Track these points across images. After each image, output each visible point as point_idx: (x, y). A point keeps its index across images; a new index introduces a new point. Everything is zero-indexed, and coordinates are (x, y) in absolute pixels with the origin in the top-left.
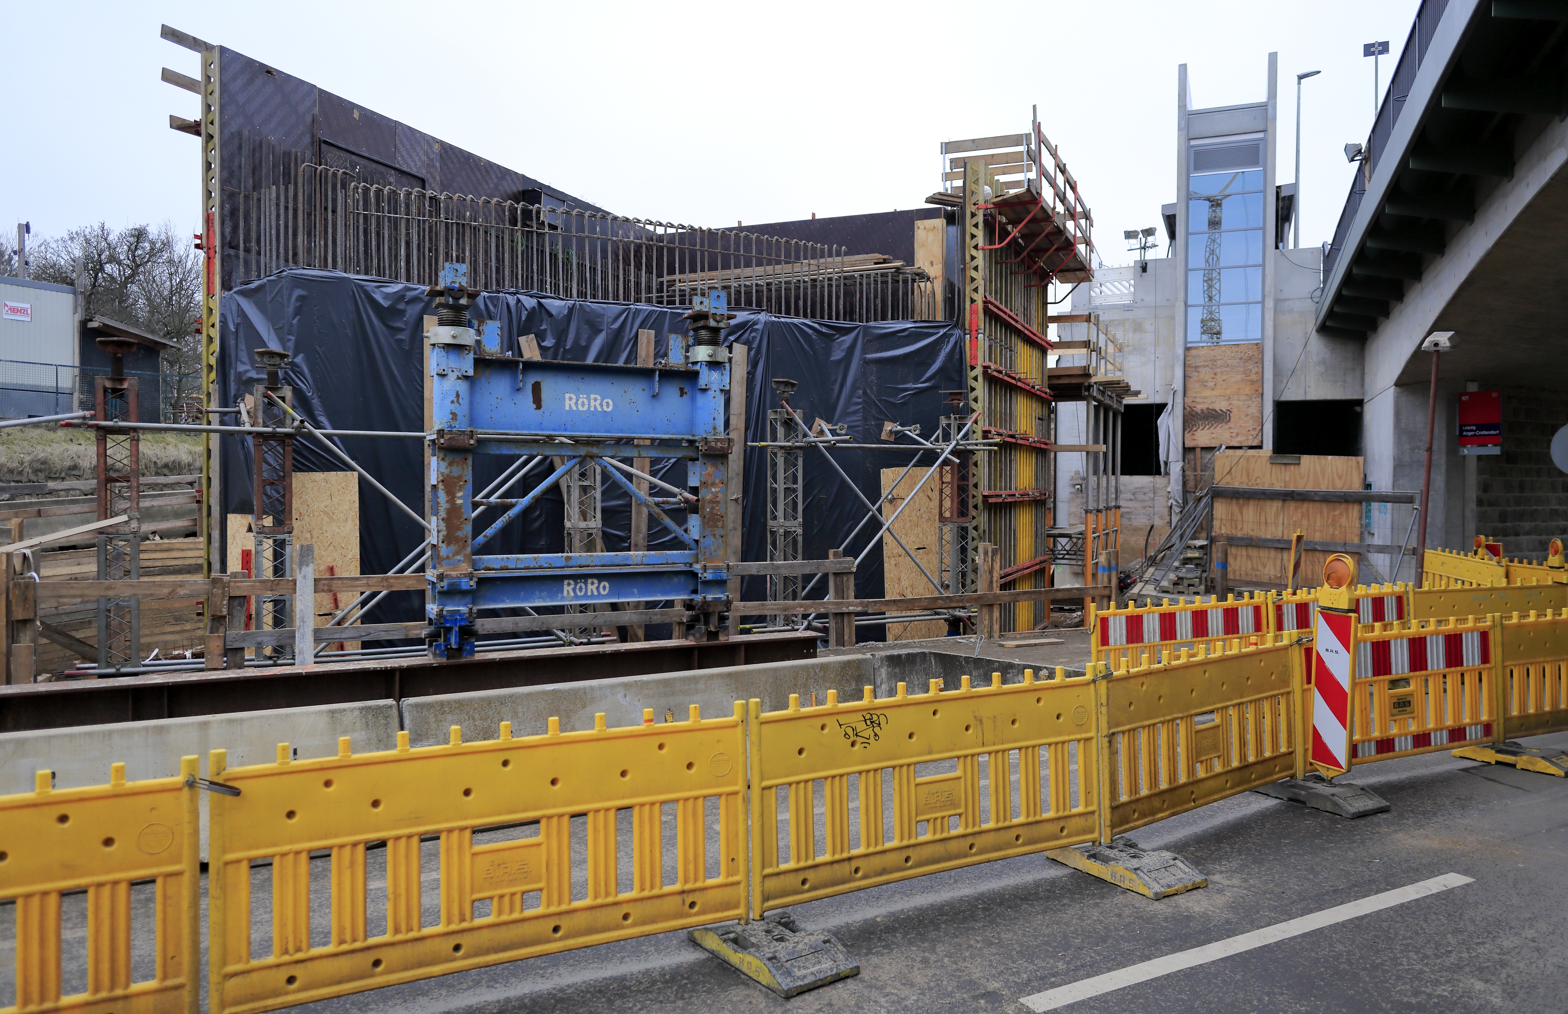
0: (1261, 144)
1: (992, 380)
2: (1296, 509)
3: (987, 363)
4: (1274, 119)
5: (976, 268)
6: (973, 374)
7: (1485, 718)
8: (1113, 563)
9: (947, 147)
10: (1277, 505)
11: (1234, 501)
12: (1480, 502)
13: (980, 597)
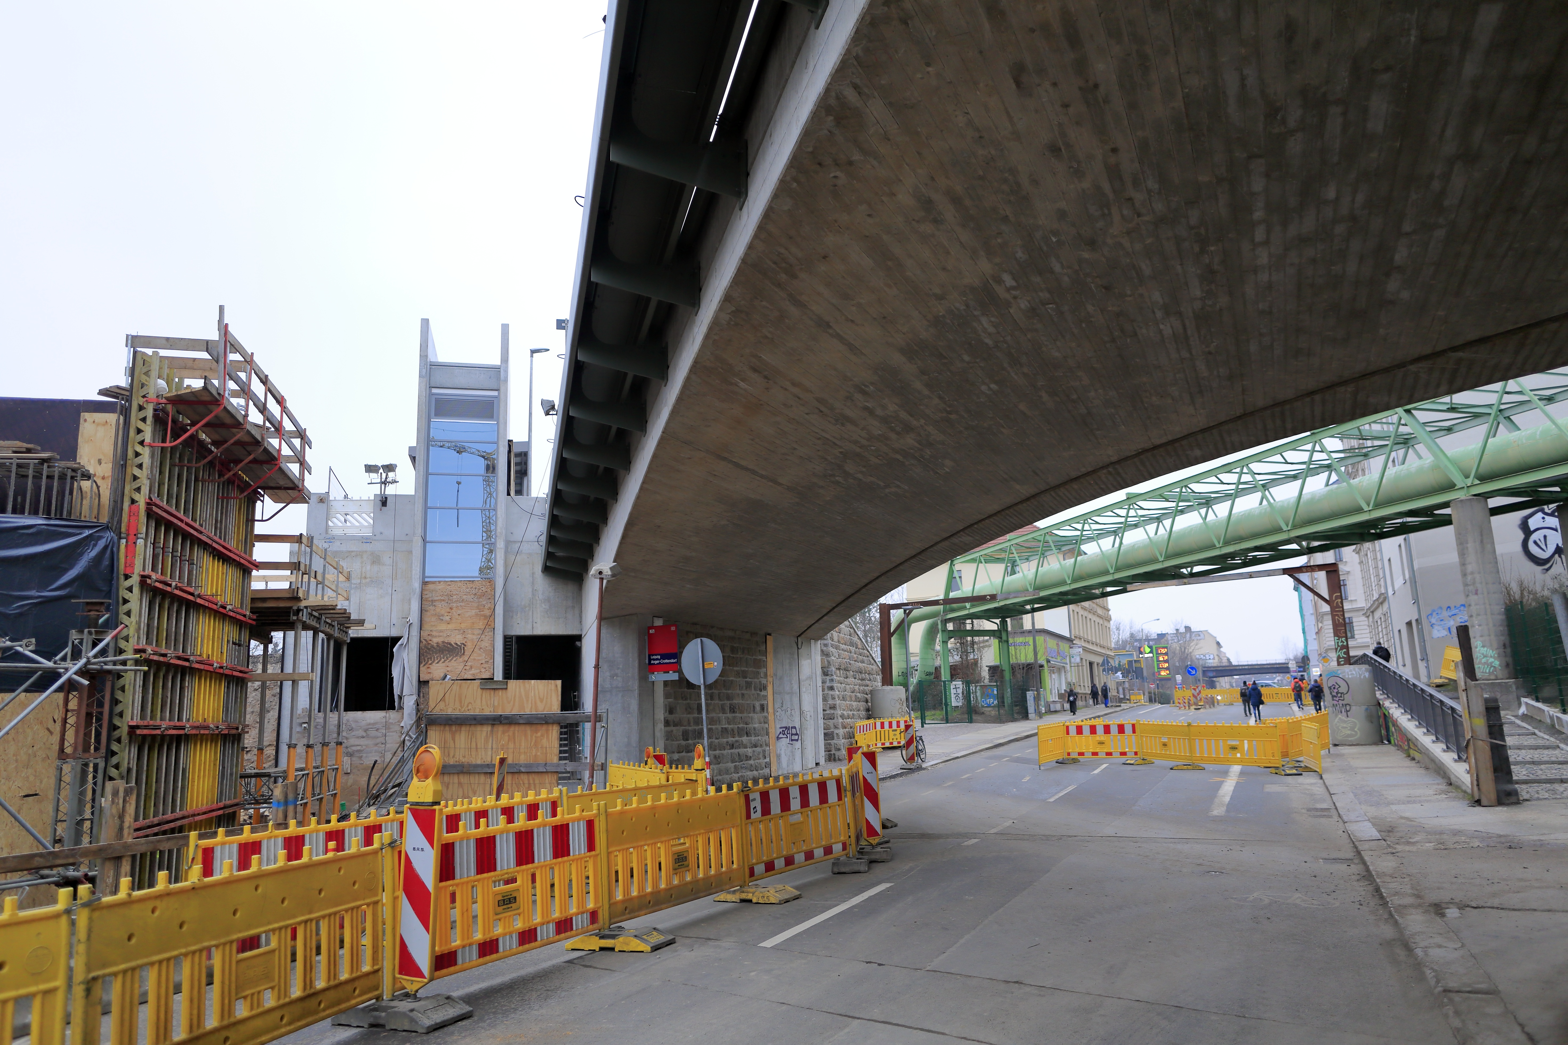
0: (496, 400)
1: (156, 594)
2: (504, 733)
3: (148, 571)
4: (506, 380)
5: (140, 466)
6: (128, 583)
7: (591, 906)
8: (291, 797)
9: (134, 341)
10: (487, 729)
11: (447, 728)
12: (667, 723)
13: (101, 850)
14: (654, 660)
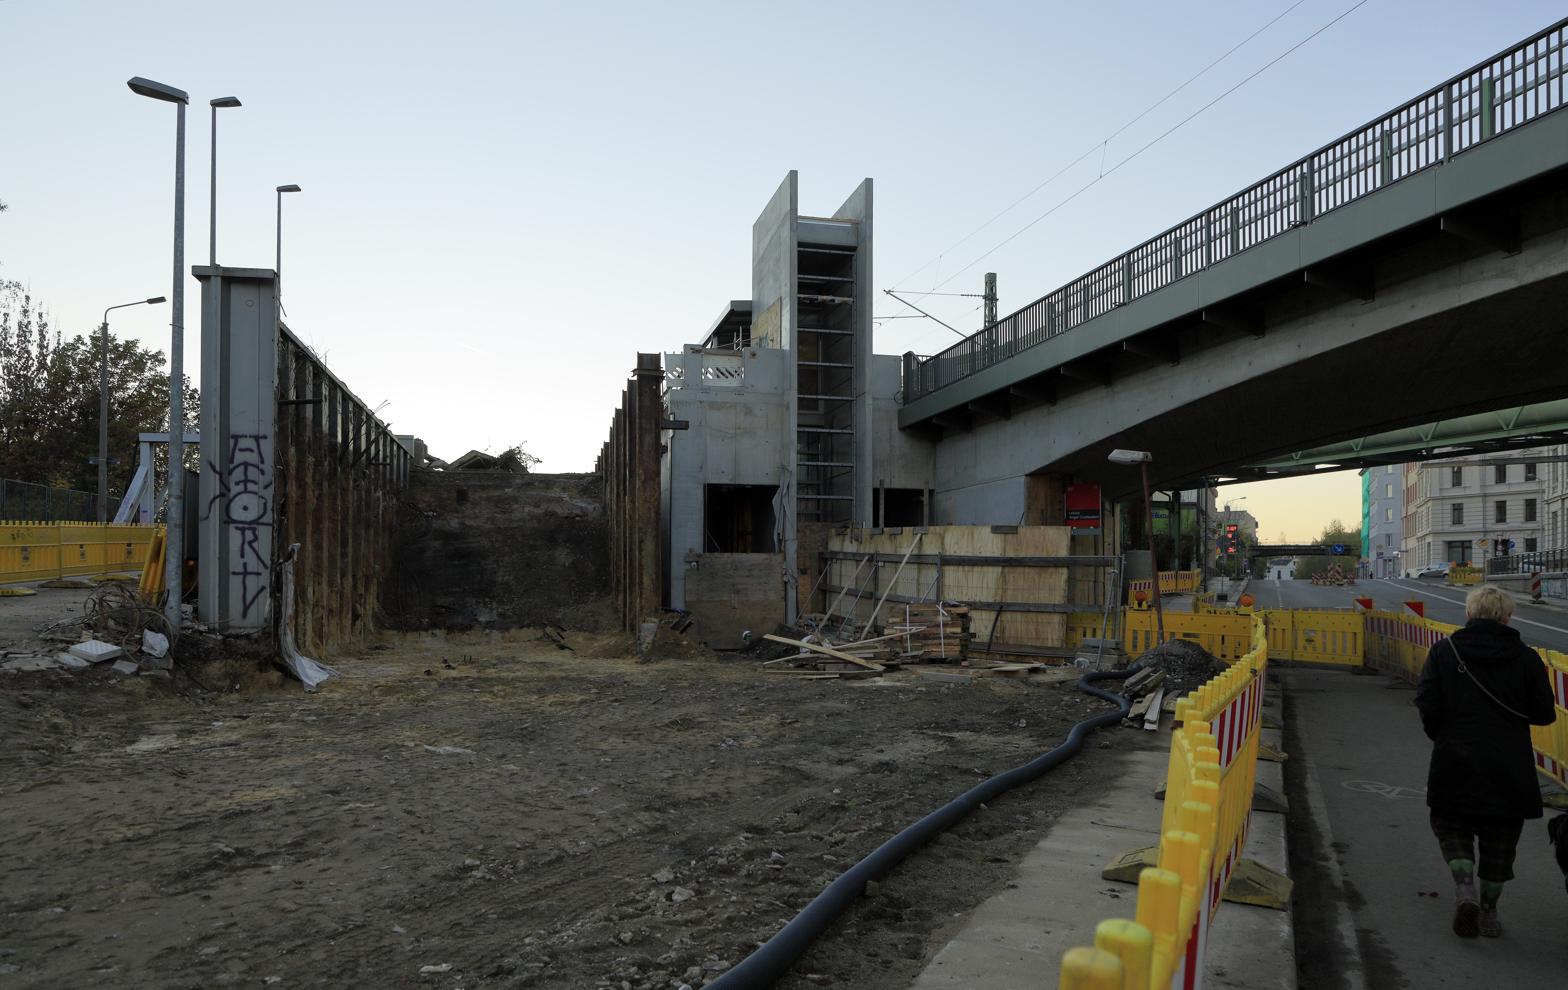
11: (961, 568)
14: (1072, 515)
